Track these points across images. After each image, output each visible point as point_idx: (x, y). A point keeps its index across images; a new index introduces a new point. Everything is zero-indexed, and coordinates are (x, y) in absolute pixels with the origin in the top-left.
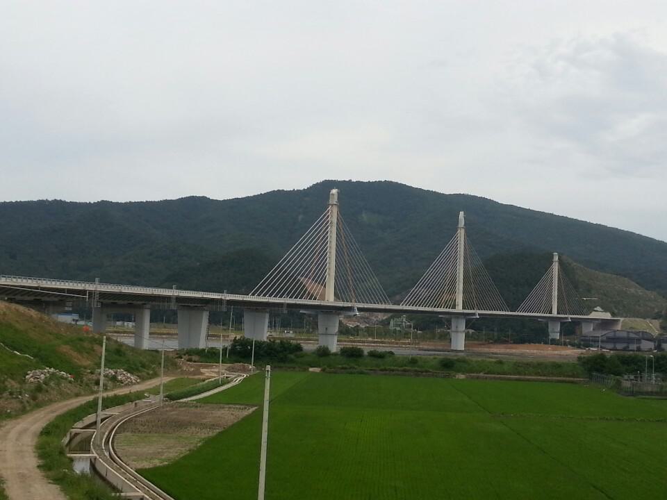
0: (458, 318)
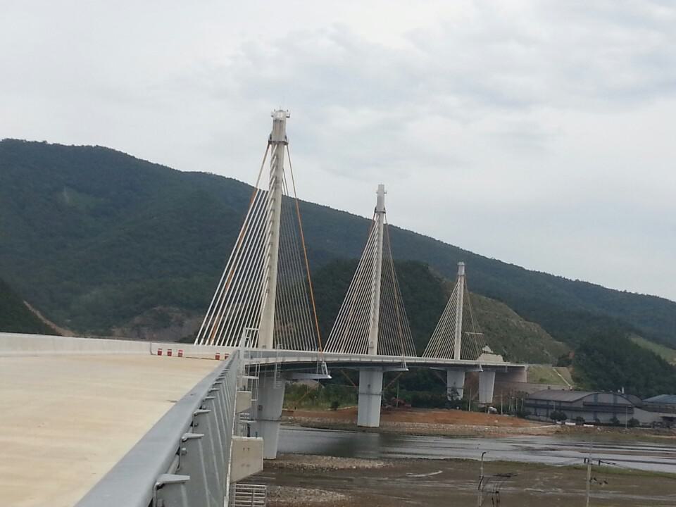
0: (373, 370)
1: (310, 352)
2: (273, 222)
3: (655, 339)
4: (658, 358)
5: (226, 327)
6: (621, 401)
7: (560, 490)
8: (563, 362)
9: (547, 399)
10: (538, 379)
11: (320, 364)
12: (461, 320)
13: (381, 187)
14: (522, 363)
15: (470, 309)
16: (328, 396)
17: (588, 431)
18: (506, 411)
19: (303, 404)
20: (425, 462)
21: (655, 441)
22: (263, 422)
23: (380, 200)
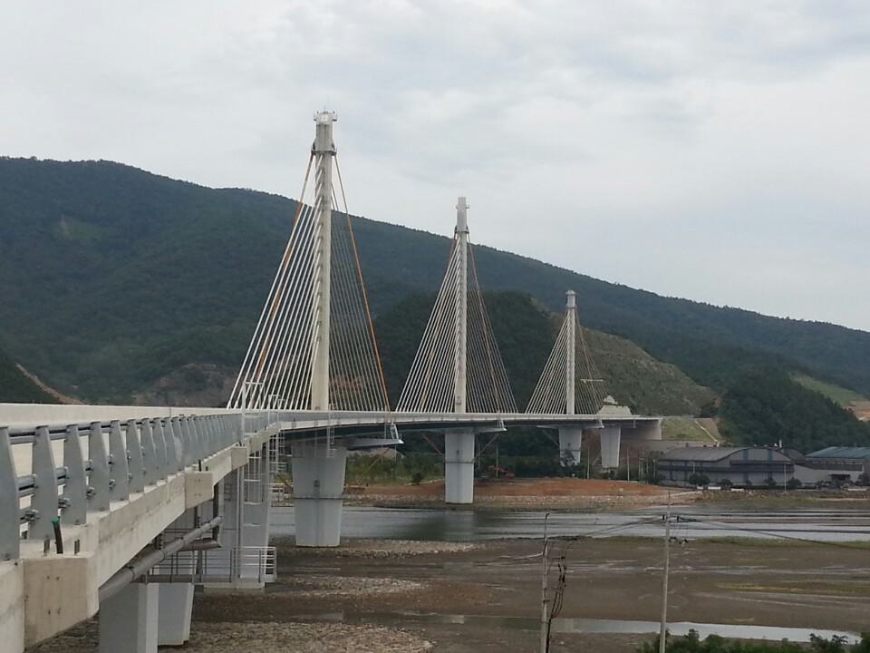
0: (461, 432)
1: (378, 412)
2: (322, 252)
3: (826, 378)
4: (828, 402)
5: (278, 385)
6: (777, 457)
7: (689, 567)
8: (707, 412)
9: (686, 459)
10: (674, 435)
11: (389, 427)
12: (573, 364)
13: (462, 201)
14: (654, 416)
15: (585, 348)
16: (408, 467)
17: (736, 497)
18: (634, 476)
19: (376, 479)
20: (525, 541)
21: (820, 505)
22: (326, 503)
23: (461, 217)
